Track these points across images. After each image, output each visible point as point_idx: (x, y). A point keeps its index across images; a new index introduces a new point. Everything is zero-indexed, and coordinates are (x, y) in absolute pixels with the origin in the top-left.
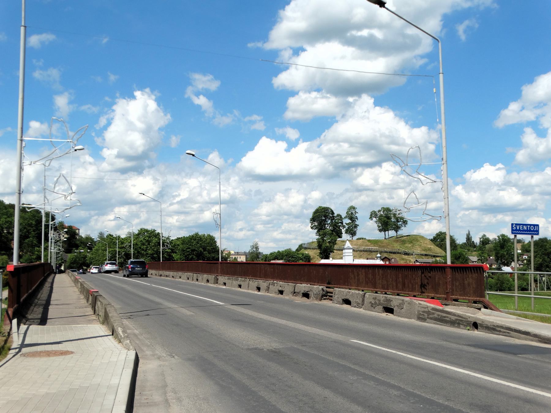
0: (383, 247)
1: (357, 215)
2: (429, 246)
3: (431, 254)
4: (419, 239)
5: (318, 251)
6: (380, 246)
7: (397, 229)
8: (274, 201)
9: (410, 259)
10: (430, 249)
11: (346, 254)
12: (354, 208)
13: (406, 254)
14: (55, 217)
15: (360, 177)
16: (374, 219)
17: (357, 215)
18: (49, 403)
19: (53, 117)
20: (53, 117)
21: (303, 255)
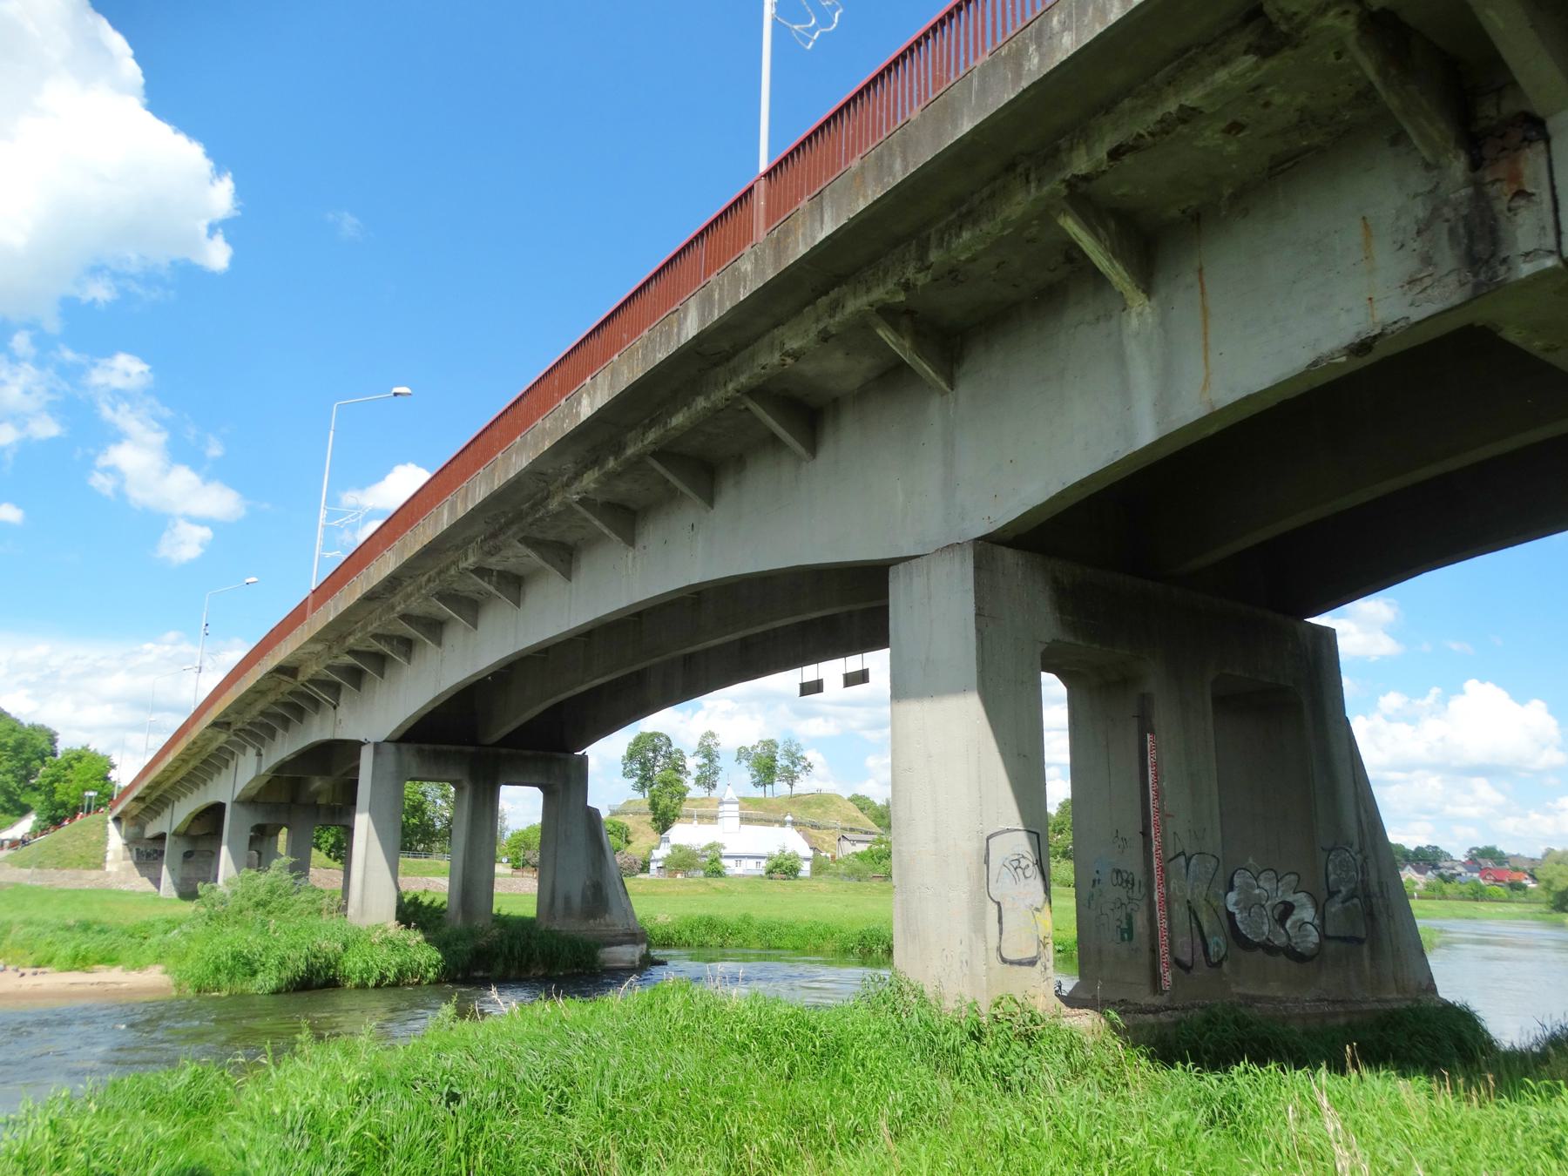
0: (772, 811)
1: (719, 748)
2: (855, 814)
3: (860, 828)
4: (835, 799)
5: (649, 818)
6: (766, 810)
7: (791, 779)
8: (1504, 261)
9: (823, 836)
10: (856, 820)
11: (726, 814)
12: (712, 735)
13: (814, 826)
14: (58, 737)
15: (1480, 324)
16: (745, 763)
17: (719, 748)
18: (866, 833)
19: (841, 11)
20: (841, 11)
21: (614, 826)
